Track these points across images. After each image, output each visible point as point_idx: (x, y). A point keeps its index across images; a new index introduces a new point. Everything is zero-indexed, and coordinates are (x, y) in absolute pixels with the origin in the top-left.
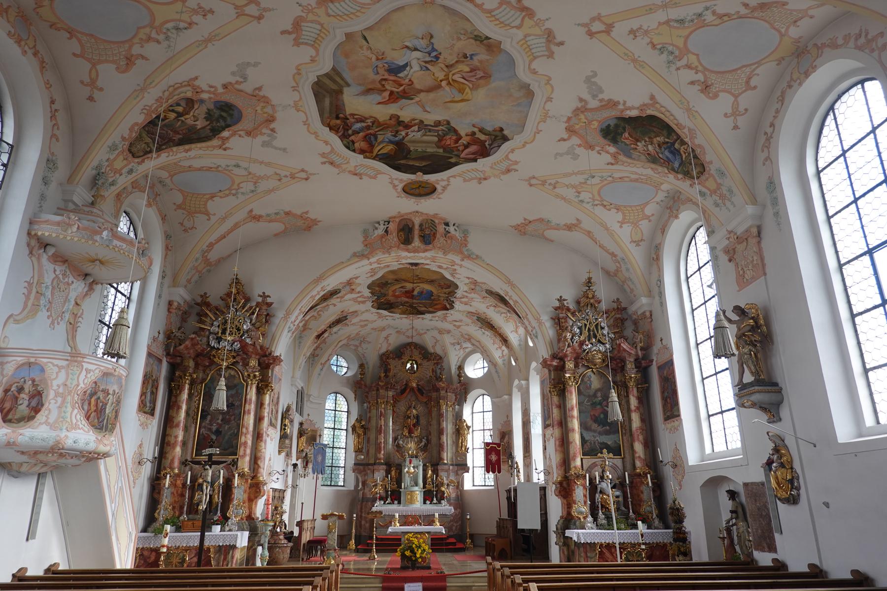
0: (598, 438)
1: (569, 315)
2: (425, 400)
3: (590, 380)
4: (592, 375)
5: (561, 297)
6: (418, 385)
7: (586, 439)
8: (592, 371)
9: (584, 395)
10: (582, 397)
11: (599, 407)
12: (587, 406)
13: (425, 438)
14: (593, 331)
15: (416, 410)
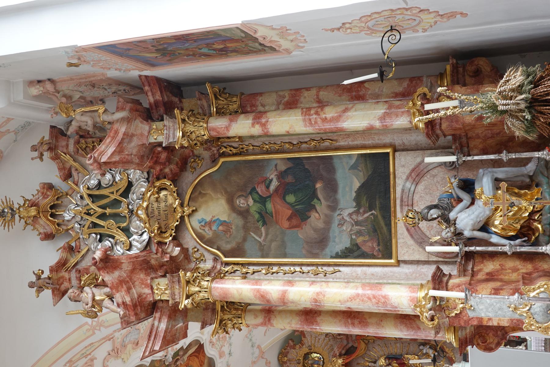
0: (345, 213)
1: (73, 261)
2: (363, 345)
3: (209, 224)
4: (199, 216)
5: (31, 285)
6: (340, 356)
7: (348, 245)
8: (189, 216)
9: (245, 240)
10: (248, 246)
11: (269, 206)
12: (269, 237)
13: (421, 347)
14: (103, 207)
15: (379, 358)
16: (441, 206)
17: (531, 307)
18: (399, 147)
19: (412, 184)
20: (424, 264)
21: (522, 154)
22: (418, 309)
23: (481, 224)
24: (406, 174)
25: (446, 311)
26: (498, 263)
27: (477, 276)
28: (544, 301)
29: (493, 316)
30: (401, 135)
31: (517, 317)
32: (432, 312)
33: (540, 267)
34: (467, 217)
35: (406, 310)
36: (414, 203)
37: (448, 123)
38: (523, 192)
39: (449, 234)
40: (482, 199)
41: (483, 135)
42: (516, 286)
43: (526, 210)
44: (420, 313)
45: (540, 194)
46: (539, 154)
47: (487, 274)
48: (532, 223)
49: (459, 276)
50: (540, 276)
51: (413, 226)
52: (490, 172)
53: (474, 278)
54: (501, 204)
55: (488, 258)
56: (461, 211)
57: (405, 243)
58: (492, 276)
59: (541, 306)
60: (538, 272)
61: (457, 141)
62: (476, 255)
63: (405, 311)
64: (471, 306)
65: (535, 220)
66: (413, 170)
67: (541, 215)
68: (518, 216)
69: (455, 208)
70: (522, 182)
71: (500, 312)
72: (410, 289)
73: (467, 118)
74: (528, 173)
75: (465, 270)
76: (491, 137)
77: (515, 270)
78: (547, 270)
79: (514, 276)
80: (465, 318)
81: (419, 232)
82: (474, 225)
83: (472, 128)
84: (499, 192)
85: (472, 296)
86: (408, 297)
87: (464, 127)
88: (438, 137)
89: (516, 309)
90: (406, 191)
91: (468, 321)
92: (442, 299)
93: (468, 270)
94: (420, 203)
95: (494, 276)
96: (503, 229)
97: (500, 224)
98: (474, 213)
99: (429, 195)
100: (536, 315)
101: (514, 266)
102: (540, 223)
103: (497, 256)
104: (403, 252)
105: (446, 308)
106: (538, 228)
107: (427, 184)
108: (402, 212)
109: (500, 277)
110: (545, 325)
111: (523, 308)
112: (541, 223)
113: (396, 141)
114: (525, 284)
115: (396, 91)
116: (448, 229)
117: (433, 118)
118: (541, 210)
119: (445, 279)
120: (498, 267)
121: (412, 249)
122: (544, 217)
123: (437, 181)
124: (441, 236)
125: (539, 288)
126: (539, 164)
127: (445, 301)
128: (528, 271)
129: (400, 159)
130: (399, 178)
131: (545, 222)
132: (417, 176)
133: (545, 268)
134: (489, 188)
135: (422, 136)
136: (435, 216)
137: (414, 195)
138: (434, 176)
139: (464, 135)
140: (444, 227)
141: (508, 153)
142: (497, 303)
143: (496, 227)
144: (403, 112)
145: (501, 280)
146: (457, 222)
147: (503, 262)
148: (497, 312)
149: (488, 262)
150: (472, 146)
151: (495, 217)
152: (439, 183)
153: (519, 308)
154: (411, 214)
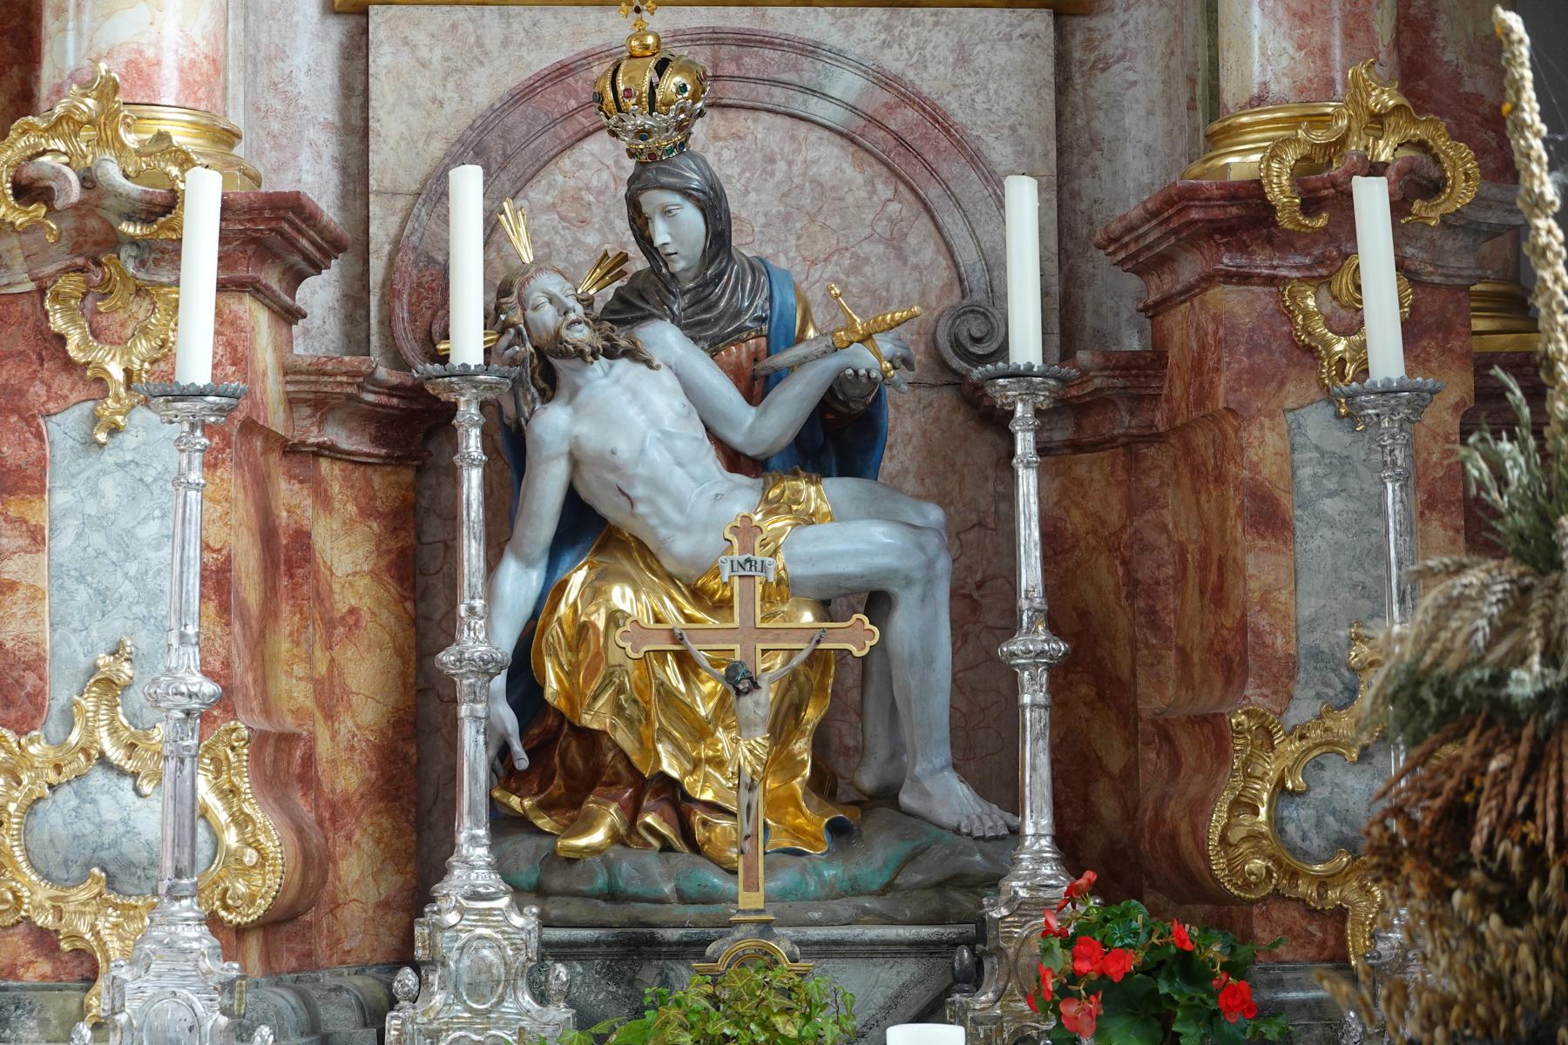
16: (720, 276)
17: (122, 772)
18: (1079, 37)
19: (853, 109)
20: (344, 169)
21: (1043, 744)
22: (90, 102)
23: (608, 507)
24: (911, 74)
25: (76, 277)
26: (366, 604)
27: (291, 477)
28: (177, 843)
29: (57, 559)
30: (1160, 49)
31: (60, 692)
32: (74, 192)
33: (349, 838)
34: (654, 422)
35: (71, 36)
36: (731, 114)
37: (1246, 321)
38: (801, 747)
39: (548, 316)
40: (768, 514)
41: (1150, 535)
42: (246, 696)
43: (696, 764)
44: (66, 118)
45: (786, 843)
46: (1037, 836)
47: (302, 538)
48: (614, 800)
49: (289, 371)
50: (300, 832)
51: (599, 98)
52: (930, 564)
53: (274, 458)
54: (748, 616)
55: (394, 545)
56: (691, 391)
57: (479, 54)
58: (288, 562)
59: (130, 831)
60: (320, 823)
61: (1119, 382)
62: (408, 476)
63: (64, 30)
64: (114, 430)
65: (633, 812)
66: (937, 118)
67: (667, 847)
68: (659, 719)
69: (706, 356)
70: (861, 752)
71: (82, 595)
72: (206, 67)
73: (1271, 438)
74: (916, 781)
75: (321, 406)
76: (1132, 582)
77: (329, 696)
78: (330, 876)
79: (294, 690)
80: (38, 389)
81: (546, 142)
82: (607, 461)
83: (1197, 471)
84: (807, 617)
85: (193, 426)
86: (157, 45)
87: (1214, 418)
88: (1148, 265)
89: (109, 686)
90: (809, 72)
91: (16, 410)
92: (169, 252)
93: (321, 423)
94: (727, 154)
95: (292, 576)
96: (583, 630)
97: (614, 618)
98: (680, 464)
99: (777, 208)
100: (74, 803)
101: (347, 692)
102: (616, 838)
103: (404, 598)
104: (420, 37)
105: (96, 279)
106: (587, 827)
107: (850, 199)
108: (696, 38)
109: (285, 609)
110: (17, 851)
111: (113, 732)
112: (618, 847)
113: (1122, 17)
114: (259, 741)
115: (1443, 21)
116: (579, 308)
117: (1521, 126)
118: (695, 848)
119: (272, 278)
120: (344, 601)
121: (440, 94)
122: (653, 862)
123: (867, 261)
124: (540, 265)
125: (242, 821)
126: (969, 842)
127: (142, 275)
128: (322, 768)
129: (1007, 39)
130: (888, 28)
131: (625, 867)
132: (900, 140)
133: (344, 865)
134: (834, 556)
135: (1146, 179)
136: (661, 234)
137: (778, 120)
138: (895, 244)
139: (1152, 425)
140: (587, 287)
141: (1050, 668)
142: (139, 579)
143: (594, 591)
144: (1324, 51)
145: (269, 612)
146: (622, 364)
147: (370, 629)
148: (81, 579)
149: (371, 546)
150: (1081, 471)
151: (652, 590)
152: (855, 269)
153: (113, 708)
154: (683, 88)
